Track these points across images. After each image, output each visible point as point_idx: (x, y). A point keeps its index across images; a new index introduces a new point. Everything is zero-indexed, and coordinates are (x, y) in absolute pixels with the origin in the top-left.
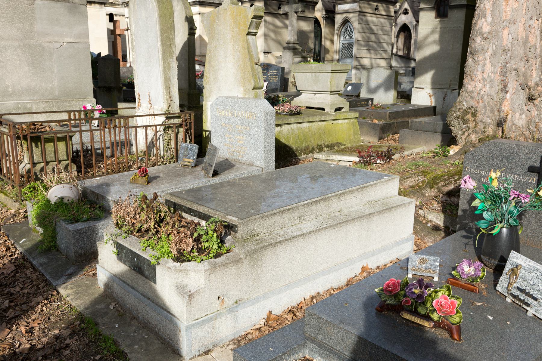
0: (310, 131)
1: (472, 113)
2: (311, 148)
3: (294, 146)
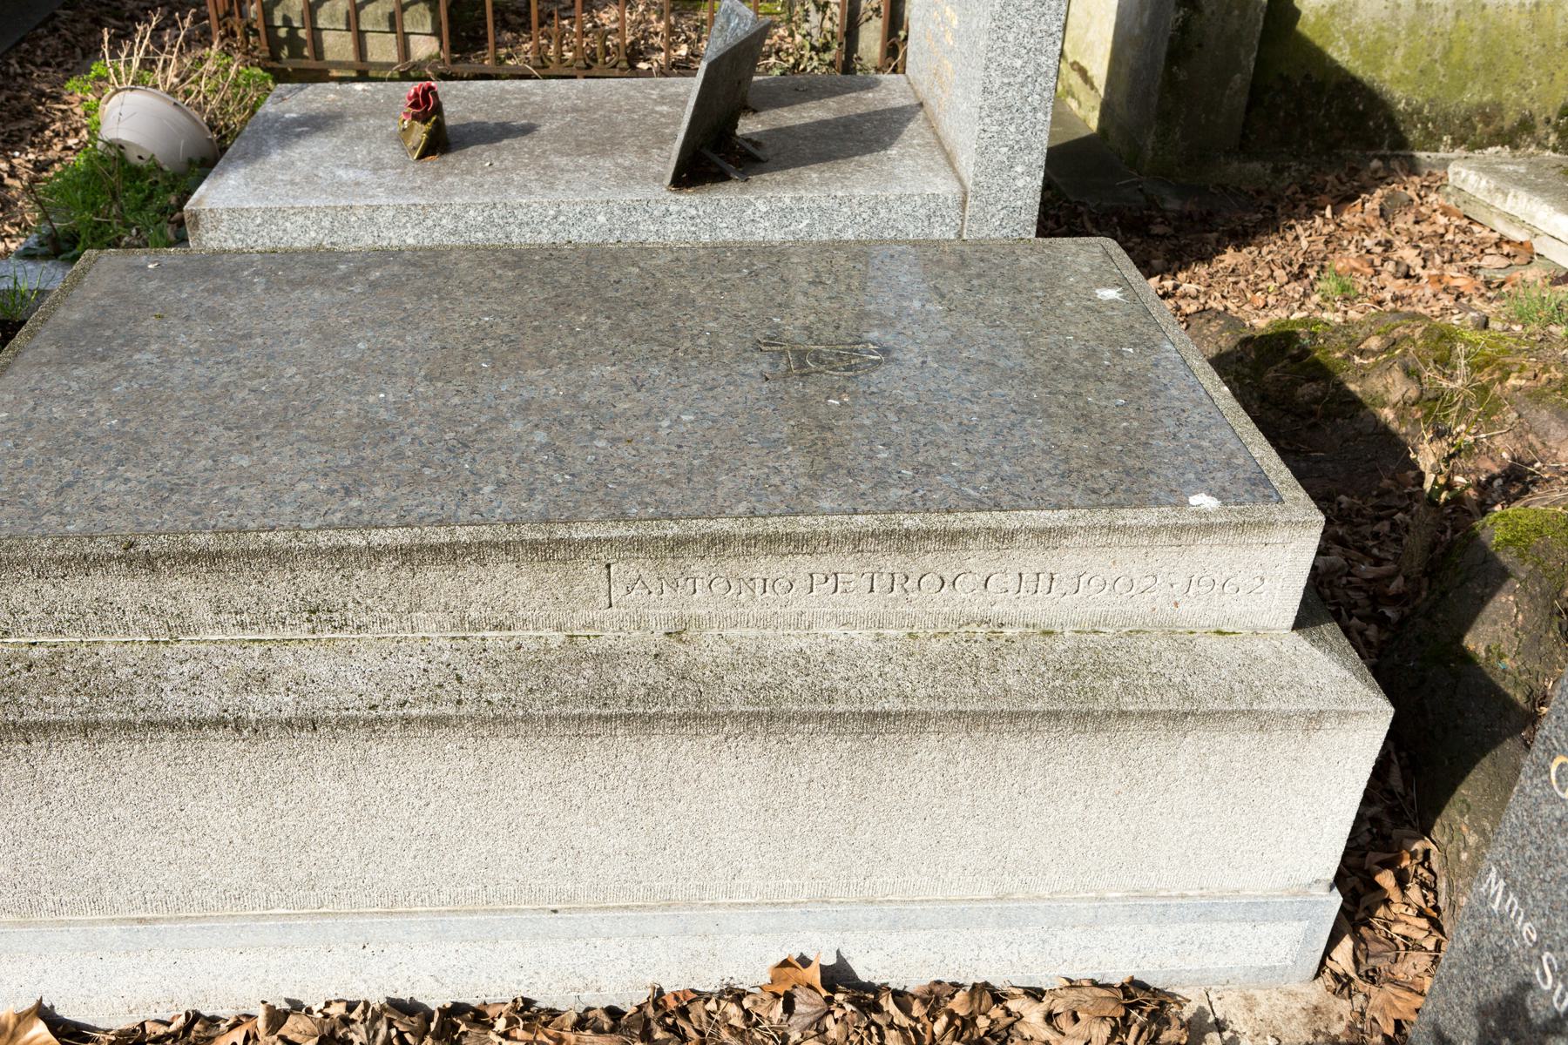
0: (1534, 27)
2: (1510, 119)
3: (1401, 96)
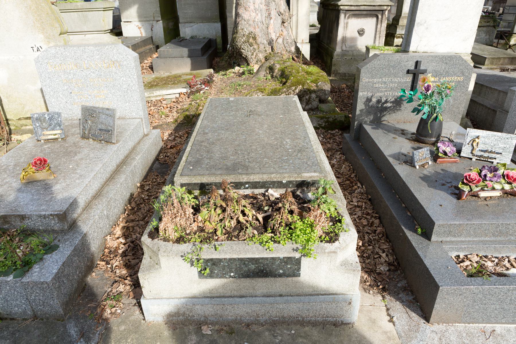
1: (253, 37)
